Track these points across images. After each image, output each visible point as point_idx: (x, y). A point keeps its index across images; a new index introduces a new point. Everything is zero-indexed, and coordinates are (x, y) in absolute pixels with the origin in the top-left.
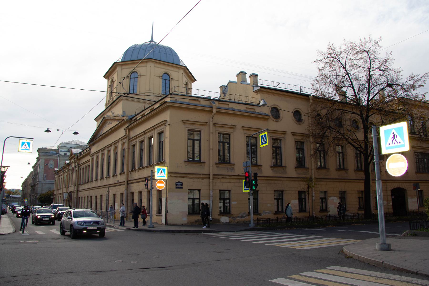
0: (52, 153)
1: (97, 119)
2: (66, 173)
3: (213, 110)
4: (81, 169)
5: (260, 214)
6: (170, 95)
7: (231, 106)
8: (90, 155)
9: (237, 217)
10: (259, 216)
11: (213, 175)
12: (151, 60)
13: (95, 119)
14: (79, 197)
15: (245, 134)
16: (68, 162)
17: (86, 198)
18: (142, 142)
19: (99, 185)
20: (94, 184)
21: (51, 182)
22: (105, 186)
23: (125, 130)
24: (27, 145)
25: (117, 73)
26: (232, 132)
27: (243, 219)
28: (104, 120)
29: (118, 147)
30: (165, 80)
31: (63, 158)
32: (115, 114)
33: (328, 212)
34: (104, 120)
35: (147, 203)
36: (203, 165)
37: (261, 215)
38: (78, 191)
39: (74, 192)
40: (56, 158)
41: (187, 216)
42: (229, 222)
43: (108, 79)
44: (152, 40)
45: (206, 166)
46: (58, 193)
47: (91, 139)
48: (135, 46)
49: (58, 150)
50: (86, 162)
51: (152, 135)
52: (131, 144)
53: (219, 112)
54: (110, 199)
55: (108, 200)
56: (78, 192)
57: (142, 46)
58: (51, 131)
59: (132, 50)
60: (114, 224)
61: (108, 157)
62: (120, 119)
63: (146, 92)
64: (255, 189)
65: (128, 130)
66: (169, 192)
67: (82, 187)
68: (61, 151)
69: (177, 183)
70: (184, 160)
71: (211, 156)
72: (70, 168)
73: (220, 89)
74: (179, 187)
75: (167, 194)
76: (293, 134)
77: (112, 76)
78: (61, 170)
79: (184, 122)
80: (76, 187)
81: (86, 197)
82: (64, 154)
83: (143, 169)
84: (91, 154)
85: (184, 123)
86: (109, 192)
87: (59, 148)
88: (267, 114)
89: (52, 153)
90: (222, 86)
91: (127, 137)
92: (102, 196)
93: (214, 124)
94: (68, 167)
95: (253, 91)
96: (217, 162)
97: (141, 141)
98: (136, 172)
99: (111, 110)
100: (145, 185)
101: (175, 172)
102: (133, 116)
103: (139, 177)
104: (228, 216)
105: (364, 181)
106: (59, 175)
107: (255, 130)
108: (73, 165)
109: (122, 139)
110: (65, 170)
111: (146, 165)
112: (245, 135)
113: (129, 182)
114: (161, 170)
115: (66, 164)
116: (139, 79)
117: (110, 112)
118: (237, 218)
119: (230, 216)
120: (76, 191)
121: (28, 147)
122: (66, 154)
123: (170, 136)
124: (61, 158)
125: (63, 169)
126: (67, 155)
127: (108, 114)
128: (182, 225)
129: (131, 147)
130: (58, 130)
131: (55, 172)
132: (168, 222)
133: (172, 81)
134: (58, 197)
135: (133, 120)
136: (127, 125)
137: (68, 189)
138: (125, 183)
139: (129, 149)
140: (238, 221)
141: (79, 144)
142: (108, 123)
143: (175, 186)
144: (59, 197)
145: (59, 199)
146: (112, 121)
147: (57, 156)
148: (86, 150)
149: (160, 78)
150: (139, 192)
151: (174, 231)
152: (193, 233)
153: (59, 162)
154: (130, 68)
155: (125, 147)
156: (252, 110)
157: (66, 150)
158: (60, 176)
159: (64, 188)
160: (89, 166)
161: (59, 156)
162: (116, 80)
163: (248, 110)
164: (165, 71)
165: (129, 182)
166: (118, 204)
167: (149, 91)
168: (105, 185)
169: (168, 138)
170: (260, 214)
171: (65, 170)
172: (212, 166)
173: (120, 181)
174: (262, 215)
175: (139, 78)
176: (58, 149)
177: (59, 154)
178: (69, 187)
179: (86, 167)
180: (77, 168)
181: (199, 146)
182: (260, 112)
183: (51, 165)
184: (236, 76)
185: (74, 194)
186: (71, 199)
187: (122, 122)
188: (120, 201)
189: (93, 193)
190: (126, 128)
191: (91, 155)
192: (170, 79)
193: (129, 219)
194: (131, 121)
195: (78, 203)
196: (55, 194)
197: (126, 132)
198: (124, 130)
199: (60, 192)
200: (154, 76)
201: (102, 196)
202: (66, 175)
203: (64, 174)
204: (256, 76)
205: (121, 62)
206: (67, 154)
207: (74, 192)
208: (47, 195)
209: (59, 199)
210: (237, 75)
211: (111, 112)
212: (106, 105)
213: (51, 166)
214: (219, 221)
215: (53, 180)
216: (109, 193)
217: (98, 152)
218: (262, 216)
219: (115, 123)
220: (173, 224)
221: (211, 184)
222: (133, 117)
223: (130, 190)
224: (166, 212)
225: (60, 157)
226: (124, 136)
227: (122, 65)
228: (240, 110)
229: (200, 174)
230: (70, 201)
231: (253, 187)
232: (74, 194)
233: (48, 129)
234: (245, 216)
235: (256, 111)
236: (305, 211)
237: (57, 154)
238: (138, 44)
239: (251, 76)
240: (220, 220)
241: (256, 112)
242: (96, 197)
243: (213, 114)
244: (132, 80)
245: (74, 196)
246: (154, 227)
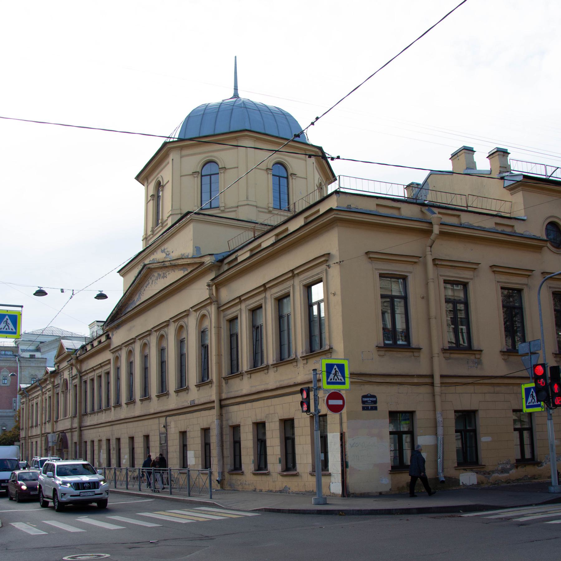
0: (5, 354)
1: (123, 272)
2: (48, 393)
3: (432, 227)
4: (86, 382)
6: (335, 194)
7: (466, 219)
8: (110, 351)
9: (493, 472)
10: (537, 468)
11: (442, 376)
13: (118, 272)
14: (86, 442)
15: (498, 282)
16: (53, 369)
17: (104, 444)
18: (255, 311)
19: (137, 413)
20: (124, 412)
21: (5, 414)
22: (156, 415)
23: (209, 285)
24: (9, 321)
25: (170, 165)
26: (472, 279)
27: (505, 475)
28: (144, 271)
29: (187, 326)
31: (27, 365)
32: (175, 255)
34: (144, 271)
35: (107, 455)
36: (416, 354)
37: (542, 466)
38: (81, 428)
39: (72, 432)
40: (13, 365)
41: (390, 473)
42: (477, 484)
43: (146, 184)
44: (236, 95)
45: (424, 356)
46: (30, 435)
47: (112, 315)
48: (205, 107)
49: (17, 347)
50: (101, 366)
51: (286, 291)
52: (224, 317)
53: (447, 232)
54: (170, 443)
55: (166, 445)
56: (81, 431)
57: (220, 106)
58: (47, 292)
59: (200, 115)
60: (211, 498)
61: (159, 351)
62: (189, 264)
63: (240, 204)
65: (214, 287)
66: (348, 420)
67: (89, 421)
68: (23, 351)
69: (364, 397)
70: (376, 345)
71: (434, 333)
72: (58, 381)
74: (370, 406)
75: (345, 425)
77: (158, 174)
78: (36, 387)
79: (371, 256)
80: (76, 420)
81: (104, 439)
82: (29, 357)
83: (266, 371)
84: (112, 347)
85: (370, 258)
86: (168, 427)
87: (19, 343)
88: (540, 237)
89: (5, 354)
90: (412, 184)
91: (211, 301)
92: (147, 437)
93: (434, 260)
94: (52, 380)
95: (504, 188)
96: (445, 348)
97: (251, 309)
98: (244, 380)
99: (163, 248)
100: (302, 403)
101: (359, 372)
102: (225, 255)
103: (254, 390)
104: (474, 470)
106: (30, 397)
108: (66, 375)
109: (199, 307)
110: (45, 385)
111: (273, 361)
112: (499, 284)
113: (223, 403)
114: (335, 367)
115: (47, 373)
116: (221, 176)
117: (159, 251)
118: (493, 475)
119: (479, 469)
120: (77, 429)
121: (11, 326)
122: (32, 357)
123: (343, 288)
124: (24, 365)
125: (40, 384)
126: (35, 358)
127: (152, 257)
128: (381, 495)
129: (224, 325)
130: (62, 291)
131: (21, 392)
132: (351, 490)
133: (294, 180)
134: (30, 444)
135: (227, 263)
136: (212, 276)
137: (55, 426)
138: (216, 405)
139: (218, 328)
140: (496, 481)
141: (58, 335)
142: (154, 276)
143: (361, 405)
144: (34, 443)
145: (34, 446)
146: (165, 272)
147: (16, 360)
148: (98, 340)
149: (268, 174)
150: (254, 423)
151: (392, 509)
152: (449, 514)
153: (21, 372)
154: (200, 153)
155: (206, 323)
156: (508, 230)
157: (32, 348)
158: (33, 400)
159: (45, 423)
160: (108, 373)
161: (19, 360)
162: (168, 182)
163: (500, 229)
165: (223, 403)
166: (195, 454)
167: (246, 203)
168: (156, 411)
169: (339, 292)
171: (45, 385)
172: (437, 355)
173: (197, 402)
174: (544, 464)
175: (222, 174)
176: (15, 347)
177: (19, 355)
178: (59, 422)
179: (100, 377)
180: (76, 381)
181: (405, 312)
182: (525, 231)
183: (5, 379)
184: (450, 159)
185: (72, 436)
186: (66, 447)
187: (199, 270)
188: (200, 445)
189: (104, 433)
190: (210, 281)
191: (112, 349)
192: (289, 174)
193: (230, 485)
194: (219, 267)
195: (83, 453)
196: (24, 436)
197: (211, 290)
198: (207, 287)
199: (36, 431)
201: (147, 437)
202: (50, 397)
203: (43, 393)
204: (504, 153)
205: (180, 140)
206: (35, 355)
207: (72, 432)
208: (3, 439)
209: (34, 446)
210: (452, 157)
211: (163, 251)
212: (146, 239)
213: (4, 380)
214: (456, 481)
215: (10, 409)
216: (169, 430)
217: (132, 341)
218: (543, 467)
219: (174, 276)
220: (361, 494)
221: (438, 399)
222: (225, 256)
223: (227, 420)
224: (342, 466)
225: (21, 363)
226: (204, 301)
227: (182, 148)
228: (484, 228)
229: (412, 376)
230: (64, 450)
232: (72, 436)
233: (40, 288)
234: (511, 469)
235: (517, 231)
237: (16, 356)
238: (209, 104)
239: (494, 155)
240: (459, 480)
241: (515, 232)
242: (132, 439)
243: (433, 237)
244: (206, 180)
245: (72, 440)
246: (326, 504)
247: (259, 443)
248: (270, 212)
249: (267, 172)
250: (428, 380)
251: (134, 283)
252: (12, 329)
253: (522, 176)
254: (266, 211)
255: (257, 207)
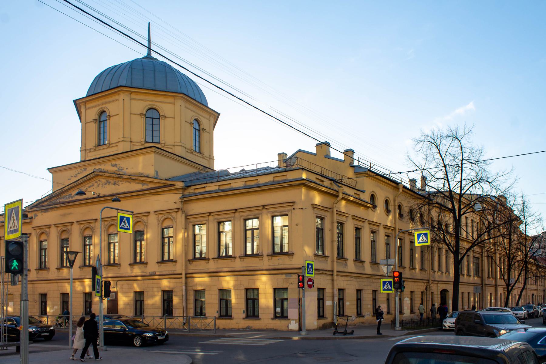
5: (363, 316)
12: (182, 95)
30: (152, 119)
33: (403, 314)
45: (329, 260)
63: (176, 144)
64: (17, 268)
73: (277, 156)
76: (385, 227)
105: (453, 283)
107: (362, 220)
113: (188, 276)
138: (184, 276)
154: (146, 100)
164: (148, 105)
170: (363, 316)
200: (174, 118)
231: (13, 262)
236: (414, 313)
243: (339, 199)
247: (135, 294)
248: (192, 153)
249: (191, 125)
250: (331, 273)
251: (77, 183)
252: (128, 227)
253: (367, 170)
254: (189, 151)
255: (186, 148)
